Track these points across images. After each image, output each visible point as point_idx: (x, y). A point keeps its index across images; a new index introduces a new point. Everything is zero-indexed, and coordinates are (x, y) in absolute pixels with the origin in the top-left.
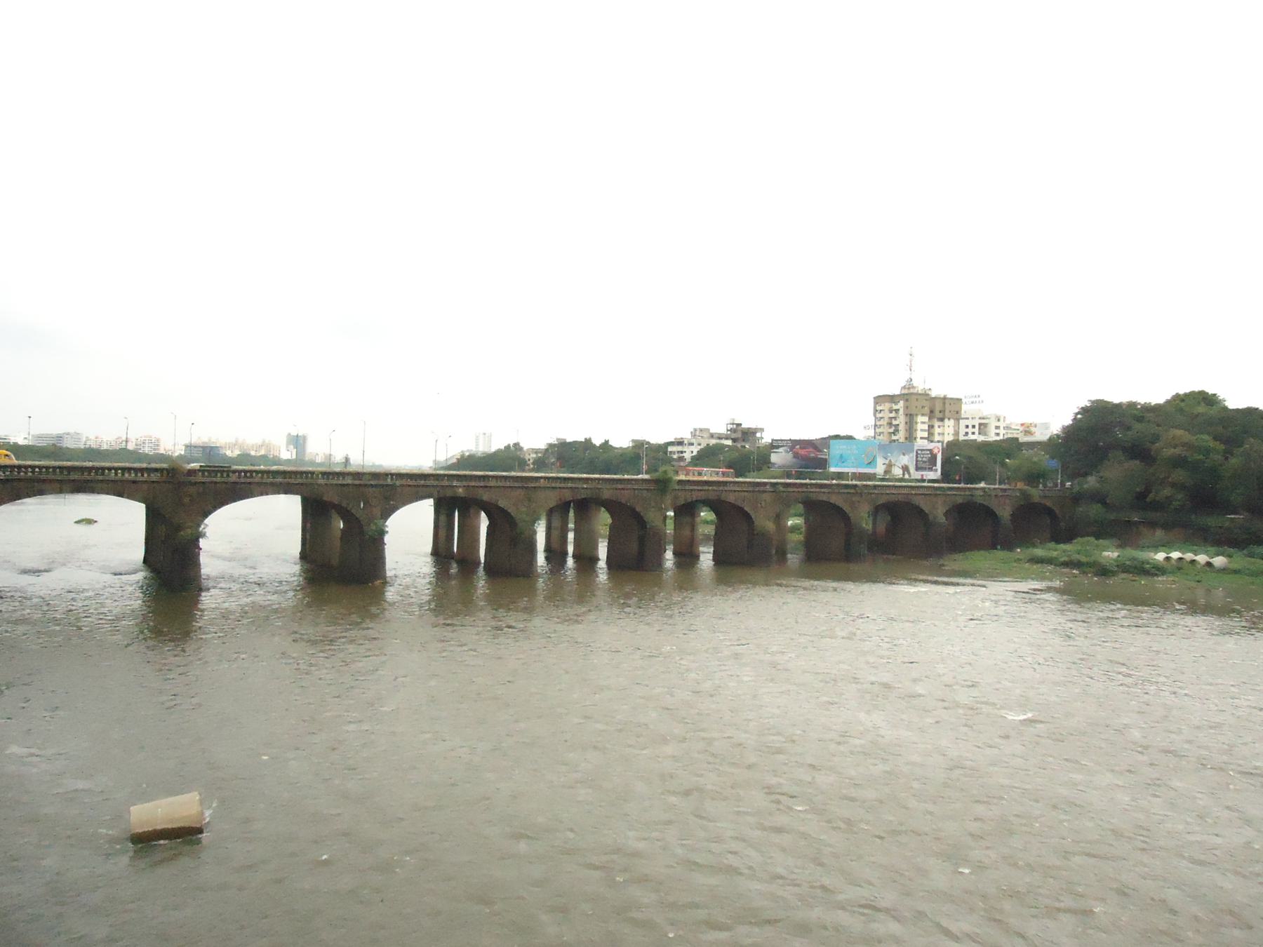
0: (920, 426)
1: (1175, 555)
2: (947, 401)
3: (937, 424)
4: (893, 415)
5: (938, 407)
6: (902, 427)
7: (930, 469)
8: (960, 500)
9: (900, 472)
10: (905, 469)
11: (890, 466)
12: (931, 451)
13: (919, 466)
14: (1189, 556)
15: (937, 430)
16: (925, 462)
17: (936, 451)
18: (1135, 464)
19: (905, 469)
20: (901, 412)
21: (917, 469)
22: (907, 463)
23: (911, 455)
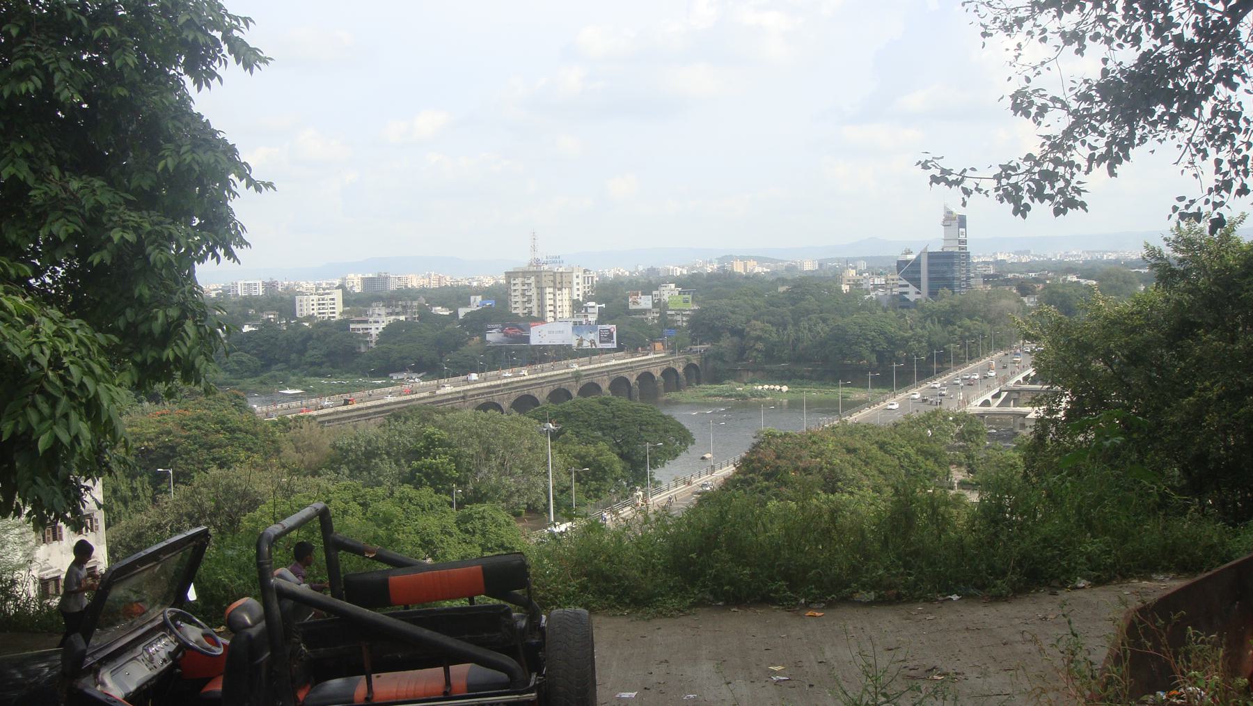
0: (548, 296)
1: (766, 387)
2: (564, 275)
3: (558, 292)
4: (525, 287)
5: (558, 279)
6: (534, 297)
8: (556, 387)
10: (592, 342)
11: (582, 340)
12: (609, 330)
13: (603, 339)
14: (772, 387)
15: (558, 298)
17: (612, 330)
18: (736, 339)
19: (592, 342)
20: (533, 285)
21: (601, 342)
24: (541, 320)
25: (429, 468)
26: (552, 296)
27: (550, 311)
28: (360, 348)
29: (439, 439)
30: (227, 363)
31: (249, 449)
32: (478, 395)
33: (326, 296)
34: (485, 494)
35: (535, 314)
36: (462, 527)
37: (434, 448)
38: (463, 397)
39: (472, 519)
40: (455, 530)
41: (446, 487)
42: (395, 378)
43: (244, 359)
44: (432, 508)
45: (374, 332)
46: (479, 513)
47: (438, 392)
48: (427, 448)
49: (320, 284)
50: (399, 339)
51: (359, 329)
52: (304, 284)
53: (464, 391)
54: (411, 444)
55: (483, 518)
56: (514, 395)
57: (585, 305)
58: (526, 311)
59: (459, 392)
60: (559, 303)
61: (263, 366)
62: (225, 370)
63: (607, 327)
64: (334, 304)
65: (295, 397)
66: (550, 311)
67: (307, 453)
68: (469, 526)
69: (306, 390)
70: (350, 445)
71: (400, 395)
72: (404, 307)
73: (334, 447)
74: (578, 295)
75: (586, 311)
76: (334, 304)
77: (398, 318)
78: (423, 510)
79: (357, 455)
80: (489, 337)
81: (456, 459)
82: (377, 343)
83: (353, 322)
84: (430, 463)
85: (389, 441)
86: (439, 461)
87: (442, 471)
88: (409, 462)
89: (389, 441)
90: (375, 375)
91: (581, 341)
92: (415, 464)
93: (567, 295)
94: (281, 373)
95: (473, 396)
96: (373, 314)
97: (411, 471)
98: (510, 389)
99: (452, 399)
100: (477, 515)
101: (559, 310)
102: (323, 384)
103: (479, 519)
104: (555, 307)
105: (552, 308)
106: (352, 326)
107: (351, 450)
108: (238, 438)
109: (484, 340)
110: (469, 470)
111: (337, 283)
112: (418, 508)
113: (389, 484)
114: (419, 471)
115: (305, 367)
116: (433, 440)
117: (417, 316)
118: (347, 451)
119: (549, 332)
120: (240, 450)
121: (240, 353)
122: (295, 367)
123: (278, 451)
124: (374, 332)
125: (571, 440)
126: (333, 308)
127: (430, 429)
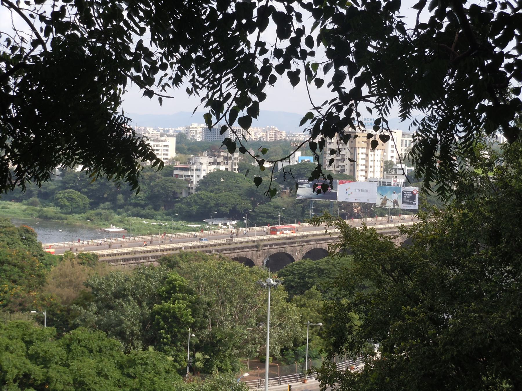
7: (412, 203)
9: (392, 204)
10: (396, 202)
12: (412, 192)
13: (405, 200)
15: (371, 158)
16: (408, 199)
17: (415, 192)
19: (396, 202)
21: (403, 203)
22: (396, 199)
23: (399, 194)
24: (352, 178)
25: (167, 311)
26: (364, 156)
27: (362, 170)
28: (181, 193)
29: (180, 285)
30: (58, 199)
31: (14, 281)
32: (271, 245)
33: (160, 143)
34: (220, 340)
35: (347, 172)
36: (126, 371)
37: (174, 293)
38: (256, 247)
39: (135, 364)
40: (116, 374)
41: (182, 330)
42: (210, 223)
43: (74, 196)
44: (100, 351)
45: (195, 179)
46: (142, 359)
47: (235, 240)
48: (168, 292)
49: (168, 131)
50: (217, 187)
51: (181, 176)
52: (150, 130)
53: (257, 241)
54: (156, 287)
55: (146, 364)
56: (307, 248)
57: (394, 167)
58: (339, 169)
59: (253, 241)
60: (370, 163)
61: (91, 204)
62: (57, 205)
63: (411, 188)
64: (167, 150)
65: (117, 234)
66: (362, 170)
67: (66, 289)
68: (131, 371)
69: (126, 229)
70: (101, 284)
71: (201, 240)
72: (225, 158)
73: (87, 285)
74: (392, 157)
75: (396, 172)
76: (167, 150)
77: (218, 167)
78: (91, 351)
79: (107, 295)
80: (300, 191)
81: (194, 306)
82: (198, 189)
83: (177, 169)
84: (169, 307)
85: (135, 284)
86: (176, 306)
87: (179, 316)
88: (150, 305)
89: (135, 284)
90: (190, 217)
91: (385, 201)
92: (156, 306)
93: (379, 156)
94: (106, 211)
95: (266, 246)
96: (195, 162)
97: (152, 313)
98: (303, 242)
99: (246, 247)
100: (140, 361)
101: (370, 169)
102: (143, 224)
103: (142, 365)
104: (367, 167)
105: (364, 168)
106: (175, 172)
107: (102, 289)
108: (5, 271)
109: (295, 195)
110: (206, 317)
111: (182, 129)
112: (85, 350)
113: (129, 323)
114: (158, 313)
115: (130, 207)
116: (174, 287)
117: (237, 167)
118: (98, 290)
119: (356, 190)
120: (6, 281)
121: (71, 190)
122: (121, 207)
123: (42, 283)
124: (195, 179)
125: (316, 295)
126: (167, 154)
127: (174, 275)
